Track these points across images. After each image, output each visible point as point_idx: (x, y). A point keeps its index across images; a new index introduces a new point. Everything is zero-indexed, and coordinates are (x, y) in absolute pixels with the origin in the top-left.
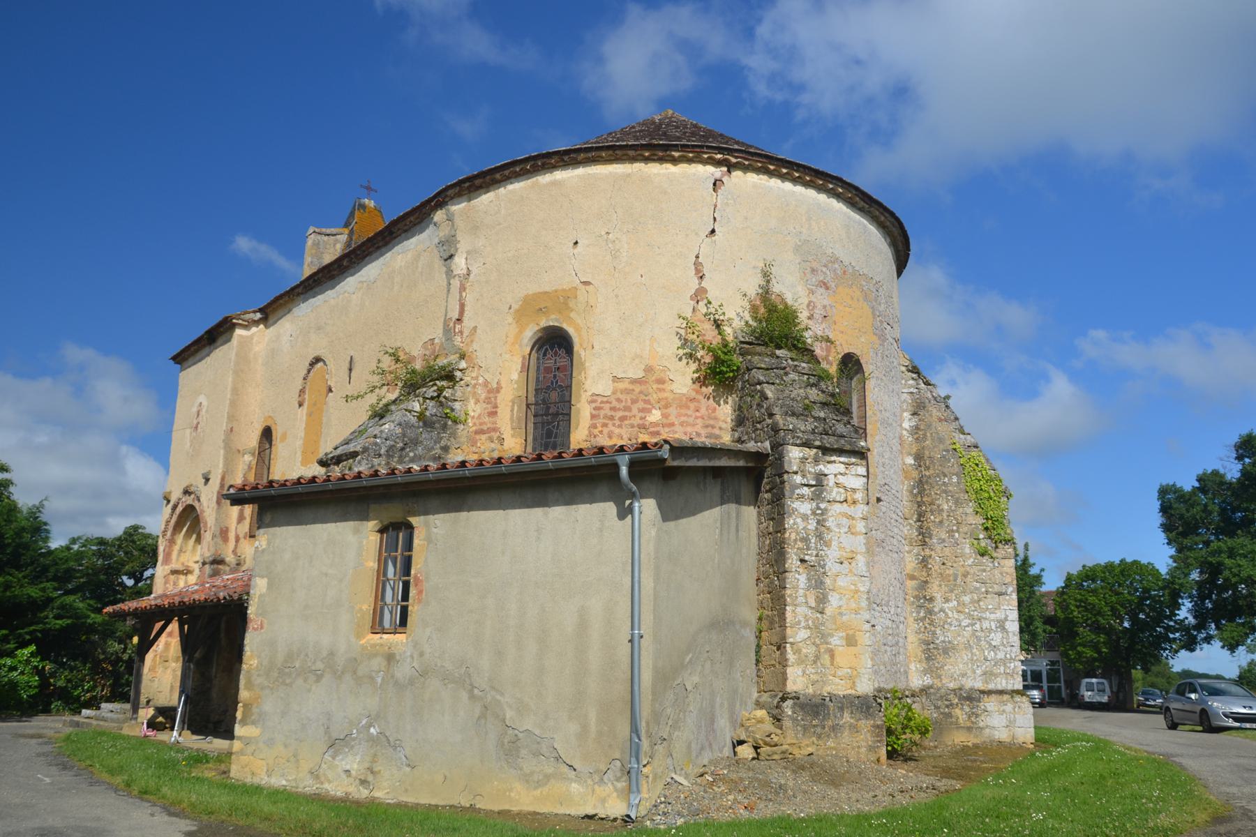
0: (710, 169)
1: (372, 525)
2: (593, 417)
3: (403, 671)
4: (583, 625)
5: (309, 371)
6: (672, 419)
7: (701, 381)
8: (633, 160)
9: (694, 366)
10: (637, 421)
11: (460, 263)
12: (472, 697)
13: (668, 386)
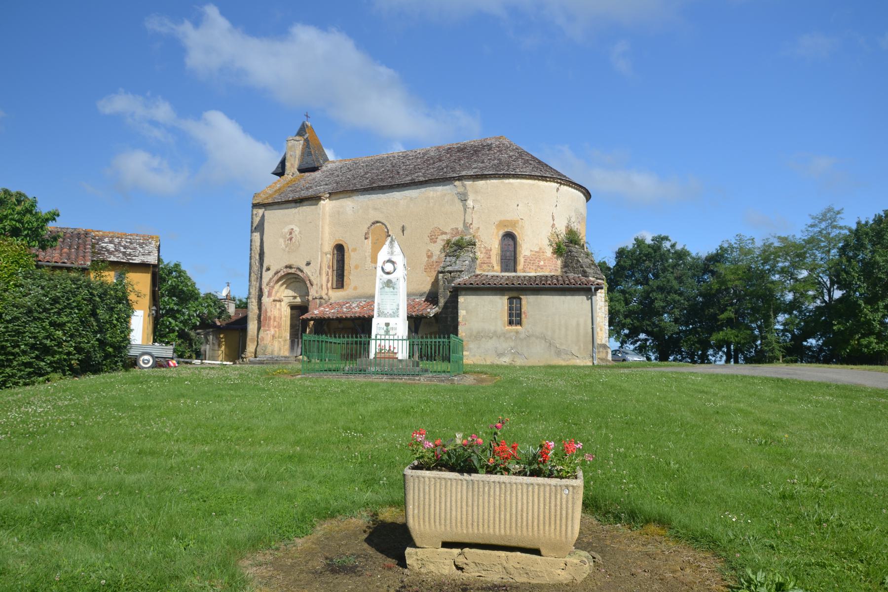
0: (556, 184)
1: (506, 297)
2: (524, 262)
3: (522, 336)
4: (578, 325)
5: (371, 226)
6: (546, 264)
7: (554, 253)
8: (535, 179)
9: (552, 248)
10: (537, 264)
11: (470, 203)
12: (546, 341)
13: (545, 254)
